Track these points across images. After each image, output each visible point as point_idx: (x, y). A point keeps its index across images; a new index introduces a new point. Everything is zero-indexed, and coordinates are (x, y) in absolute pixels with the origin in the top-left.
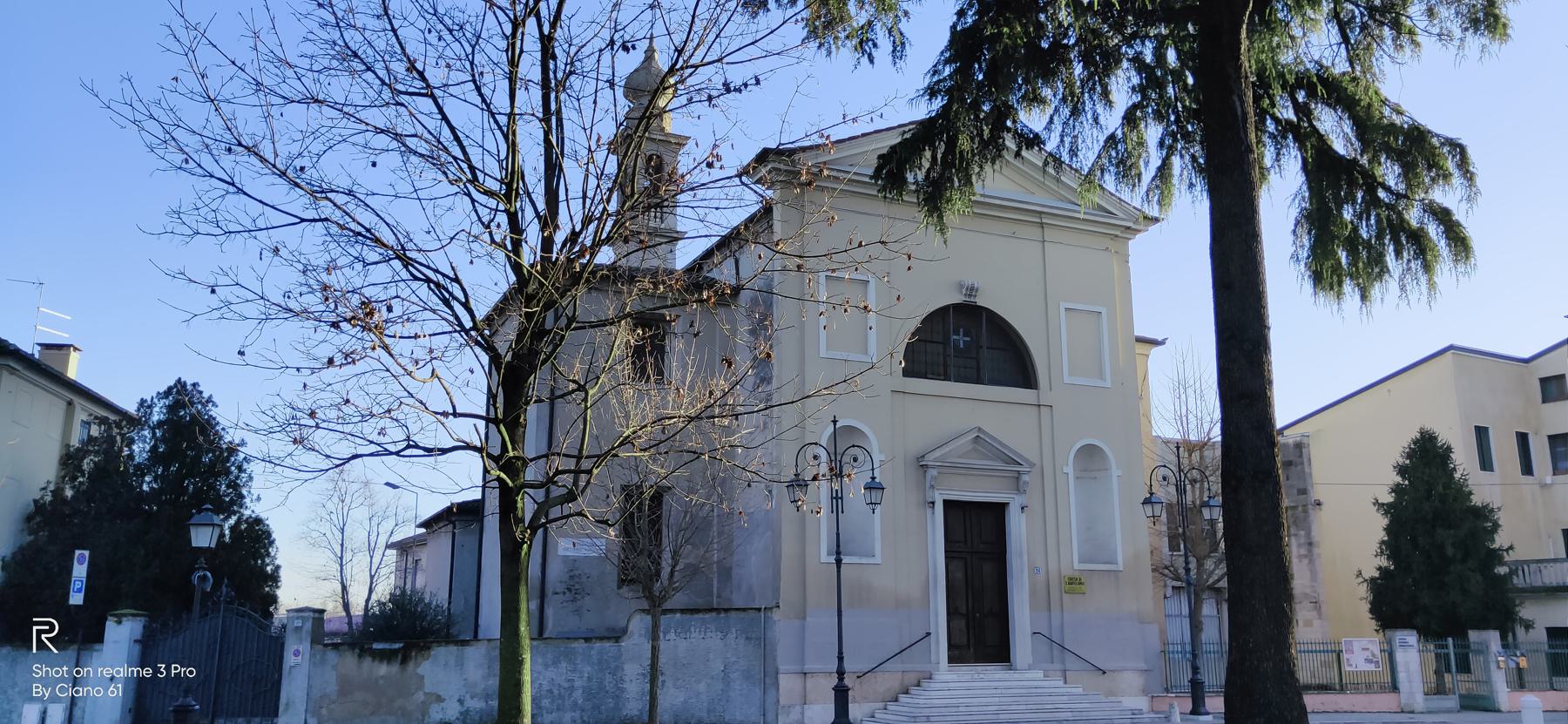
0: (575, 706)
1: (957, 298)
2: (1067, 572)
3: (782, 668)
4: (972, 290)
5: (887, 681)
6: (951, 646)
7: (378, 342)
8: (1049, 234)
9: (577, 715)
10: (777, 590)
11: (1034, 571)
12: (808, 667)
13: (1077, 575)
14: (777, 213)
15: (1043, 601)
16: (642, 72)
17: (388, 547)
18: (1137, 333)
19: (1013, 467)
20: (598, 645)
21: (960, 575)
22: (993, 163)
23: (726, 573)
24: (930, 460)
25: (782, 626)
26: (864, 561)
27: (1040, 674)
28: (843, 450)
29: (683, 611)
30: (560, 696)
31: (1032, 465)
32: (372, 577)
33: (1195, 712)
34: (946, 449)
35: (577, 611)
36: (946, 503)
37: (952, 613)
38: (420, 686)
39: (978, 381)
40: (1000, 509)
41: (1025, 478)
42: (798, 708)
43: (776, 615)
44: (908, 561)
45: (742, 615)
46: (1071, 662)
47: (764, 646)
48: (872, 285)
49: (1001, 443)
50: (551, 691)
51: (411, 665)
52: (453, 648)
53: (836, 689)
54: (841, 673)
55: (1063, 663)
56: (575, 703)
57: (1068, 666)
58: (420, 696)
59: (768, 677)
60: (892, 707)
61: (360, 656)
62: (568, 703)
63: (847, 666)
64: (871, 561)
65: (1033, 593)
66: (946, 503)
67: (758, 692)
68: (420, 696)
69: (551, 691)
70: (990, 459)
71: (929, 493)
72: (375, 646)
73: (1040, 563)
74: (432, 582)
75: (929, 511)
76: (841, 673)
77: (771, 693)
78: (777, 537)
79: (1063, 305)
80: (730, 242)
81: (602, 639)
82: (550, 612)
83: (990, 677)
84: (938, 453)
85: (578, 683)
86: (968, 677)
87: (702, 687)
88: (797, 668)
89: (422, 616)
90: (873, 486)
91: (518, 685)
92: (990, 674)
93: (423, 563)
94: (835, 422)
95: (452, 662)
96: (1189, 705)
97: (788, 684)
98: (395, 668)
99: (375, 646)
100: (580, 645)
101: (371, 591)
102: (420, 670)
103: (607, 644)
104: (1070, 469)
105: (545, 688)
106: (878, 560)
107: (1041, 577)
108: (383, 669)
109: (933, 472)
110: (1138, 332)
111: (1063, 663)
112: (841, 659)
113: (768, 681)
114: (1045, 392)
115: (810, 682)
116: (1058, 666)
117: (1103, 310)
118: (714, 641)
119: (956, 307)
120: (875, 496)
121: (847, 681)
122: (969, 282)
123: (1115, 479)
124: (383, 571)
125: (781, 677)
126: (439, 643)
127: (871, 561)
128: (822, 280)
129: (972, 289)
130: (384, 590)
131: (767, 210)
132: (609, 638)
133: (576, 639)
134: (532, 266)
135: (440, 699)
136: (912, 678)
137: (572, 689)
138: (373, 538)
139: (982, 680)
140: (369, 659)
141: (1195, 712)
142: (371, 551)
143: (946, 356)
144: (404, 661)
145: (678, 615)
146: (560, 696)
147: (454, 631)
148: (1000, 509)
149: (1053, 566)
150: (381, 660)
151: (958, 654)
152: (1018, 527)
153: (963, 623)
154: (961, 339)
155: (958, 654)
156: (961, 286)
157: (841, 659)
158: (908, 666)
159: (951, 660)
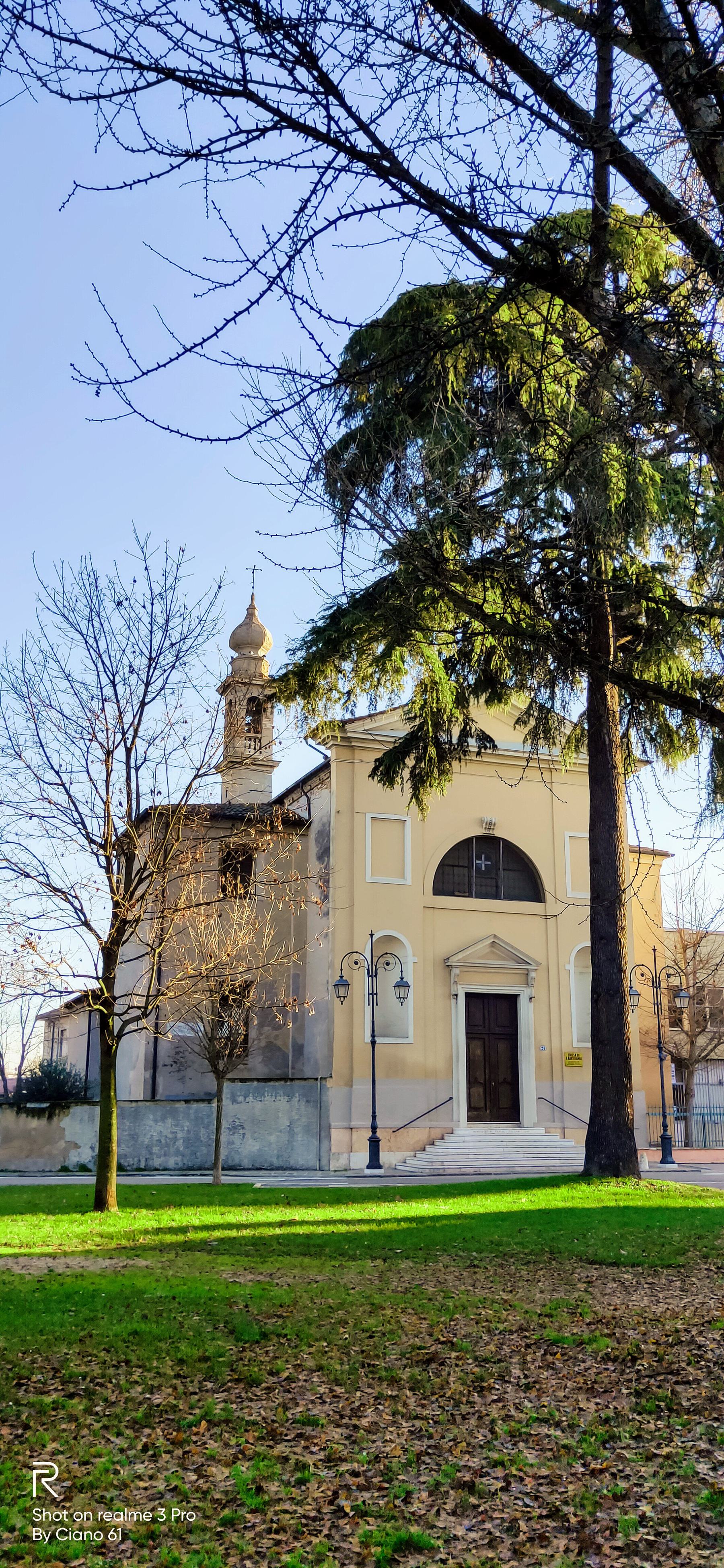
0: (178, 1153)
1: (479, 831)
2: (567, 1049)
3: (333, 1124)
4: (490, 825)
5: (416, 1135)
6: (470, 1108)
9: (179, 1159)
10: (330, 1064)
12: (353, 1124)
13: (576, 1052)
14: (333, 766)
16: (244, 628)
17: (38, 1018)
19: (524, 967)
20: (195, 1106)
21: (479, 1052)
23: (299, 1050)
24: (453, 961)
25: (334, 1091)
27: (543, 1131)
28: (384, 953)
29: (258, 1080)
30: (167, 1145)
31: (539, 964)
32: (24, 1046)
33: (663, 1161)
34: (468, 952)
35: (182, 1080)
36: (468, 995)
37: (471, 1081)
38: (62, 1137)
39: (496, 897)
40: (512, 1000)
41: (533, 974)
42: (345, 1156)
43: (329, 1083)
44: (437, 1042)
45: (303, 1083)
47: (320, 1106)
48: (408, 824)
49: (513, 947)
50: (159, 1141)
51: (55, 1119)
52: (86, 1107)
53: (370, 1140)
54: (374, 1128)
55: (563, 1121)
56: (178, 1150)
57: (567, 1124)
58: (62, 1144)
59: (323, 1131)
60: (420, 1155)
61: (17, 1113)
62: (172, 1150)
63: (379, 1123)
65: (539, 1066)
66: (468, 995)
67: (316, 1143)
68: (62, 1144)
69: (159, 1141)
70: (504, 959)
71: (453, 988)
72: (29, 1105)
73: (545, 1042)
74: (75, 1056)
75: (453, 1001)
76: (374, 1128)
77: (325, 1143)
78: (331, 1022)
79: (568, 834)
80: (302, 786)
81: (197, 1101)
82: (160, 1080)
83: (501, 1132)
84: (460, 956)
85: (180, 1135)
86: (483, 1133)
87: (273, 1138)
88: (345, 1124)
89: (64, 1083)
90: (402, 984)
91: (110, 1125)
92: (502, 1130)
93: (67, 1034)
94: (372, 935)
95: (86, 1118)
96: (659, 1155)
97: (338, 1136)
98: (44, 1122)
99: (29, 1105)
100: (181, 1106)
101: (23, 1058)
102: (62, 1124)
103: (202, 1105)
104: (571, 967)
105: (156, 1138)
106: (411, 1040)
107: (547, 1052)
108: (34, 1123)
109: (456, 971)
111: (563, 1121)
112: (374, 1117)
113: (323, 1134)
114: (551, 906)
115: (355, 1134)
116: (558, 1124)
118: (282, 1103)
119: (479, 838)
121: (379, 1134)
122: (487, 818)
124: (33, 1041)
125: (333, 1131)
126: (76, 1104)
128: (368, 820)
129: (490, 824)
130: (37, 1055)
131: (325, 766)
132: (203, 1101)
133: (179, 1101)
135: (76, 1146)
136: (436, 1133)
137: (175, 1139)
138: (25, 1012)
139: (493, 1135)
140: (24, 1115)
141: (663, 1161)
142: (23, 1023)
143: (470, 877)
144: (50, 1117)
145: (255, 1083)
146: (167, 1145)
147: (89, 1094)
148: (512, 1000)
149: (555, 1044)
150: (33, 1116)
151: (476, 1114)
152: (526, 1013)
153: (481, 1090)
154: (483, 863)
155: (476, 1114)
156: (482, 821)
157: (374, 1117)
158: (435, 1124)
159: (470, 1119)
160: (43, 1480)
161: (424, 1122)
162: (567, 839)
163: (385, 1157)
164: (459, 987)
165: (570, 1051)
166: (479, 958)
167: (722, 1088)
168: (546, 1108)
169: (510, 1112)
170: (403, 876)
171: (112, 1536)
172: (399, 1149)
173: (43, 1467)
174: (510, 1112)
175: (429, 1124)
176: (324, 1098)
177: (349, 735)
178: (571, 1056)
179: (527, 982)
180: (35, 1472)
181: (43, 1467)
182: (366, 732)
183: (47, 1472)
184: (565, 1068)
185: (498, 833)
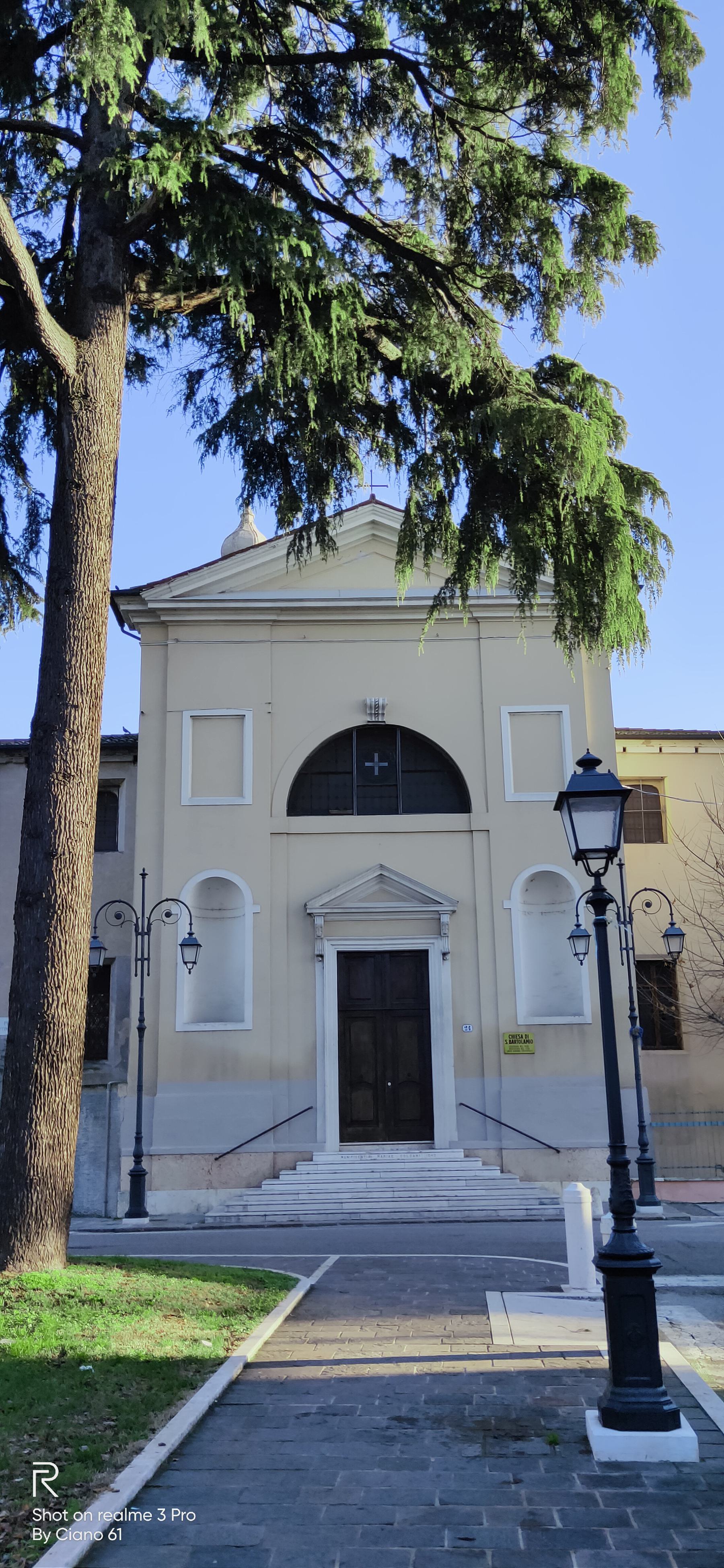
1: (360, 720)
2: (507, 1028)
4: (377, 709)
7: (353, 207)
8: (486, 629)
11: (460, 1028)
13: (522, 1031)
15: (474, 1064)
18: (617, 725)
19: (433, 910)
22: (428, 553)
24: (315, 907)
26: (230, 1026)
27: (461, 1154)
36: (344, 958)
46: (510, 1140)
48: (249, 722)
49: (411, 881)
57: (505, 1143)
64: (239, 1026)
66: (344, 958)
70: (405, 900)
75: (318, 965)
83: (387, 1157)
86: (357, 1158)
92: (396, 1158)
106: (248, 1024)
110: (620, 723)
113: (112, 1164)
116: (492, 1143)
117: (565, 709)
119: (361, 730)
120: (190, 954)
122: (371, 700)
123: (249, 920)
127: (239, 1026)
129: (377, 707)
134: (372, 373)
136: (284, 1159)
148: (420, 957)
149: (488, 1019)
151: (354, 1129)
152: (440, 978)
155: (354, 1129)
160: (43, 1480)
161: (268, 1144)
162: (506, 719)
163: (157, 1201)
164: (327, 944)
165: (513, 1030)
166: (361, 901)
167: (722, 1477)
168: (475, 1120)
169: (418, 1127)
170: (241, 794)
171: (112, 1536)
172: (225, 1185)
173: (44, 1467)
174: (418, 1127)
175: (273, 1147)
176: (114, 1113)
177: (151, 605)
178: (514, 1039)
179: (439, 931)
180: (35, 1472)
181: (44, 1467)
182: (174, 599)
183: (47, 1471)
184: (506, 1059)
185: (390, 719)
